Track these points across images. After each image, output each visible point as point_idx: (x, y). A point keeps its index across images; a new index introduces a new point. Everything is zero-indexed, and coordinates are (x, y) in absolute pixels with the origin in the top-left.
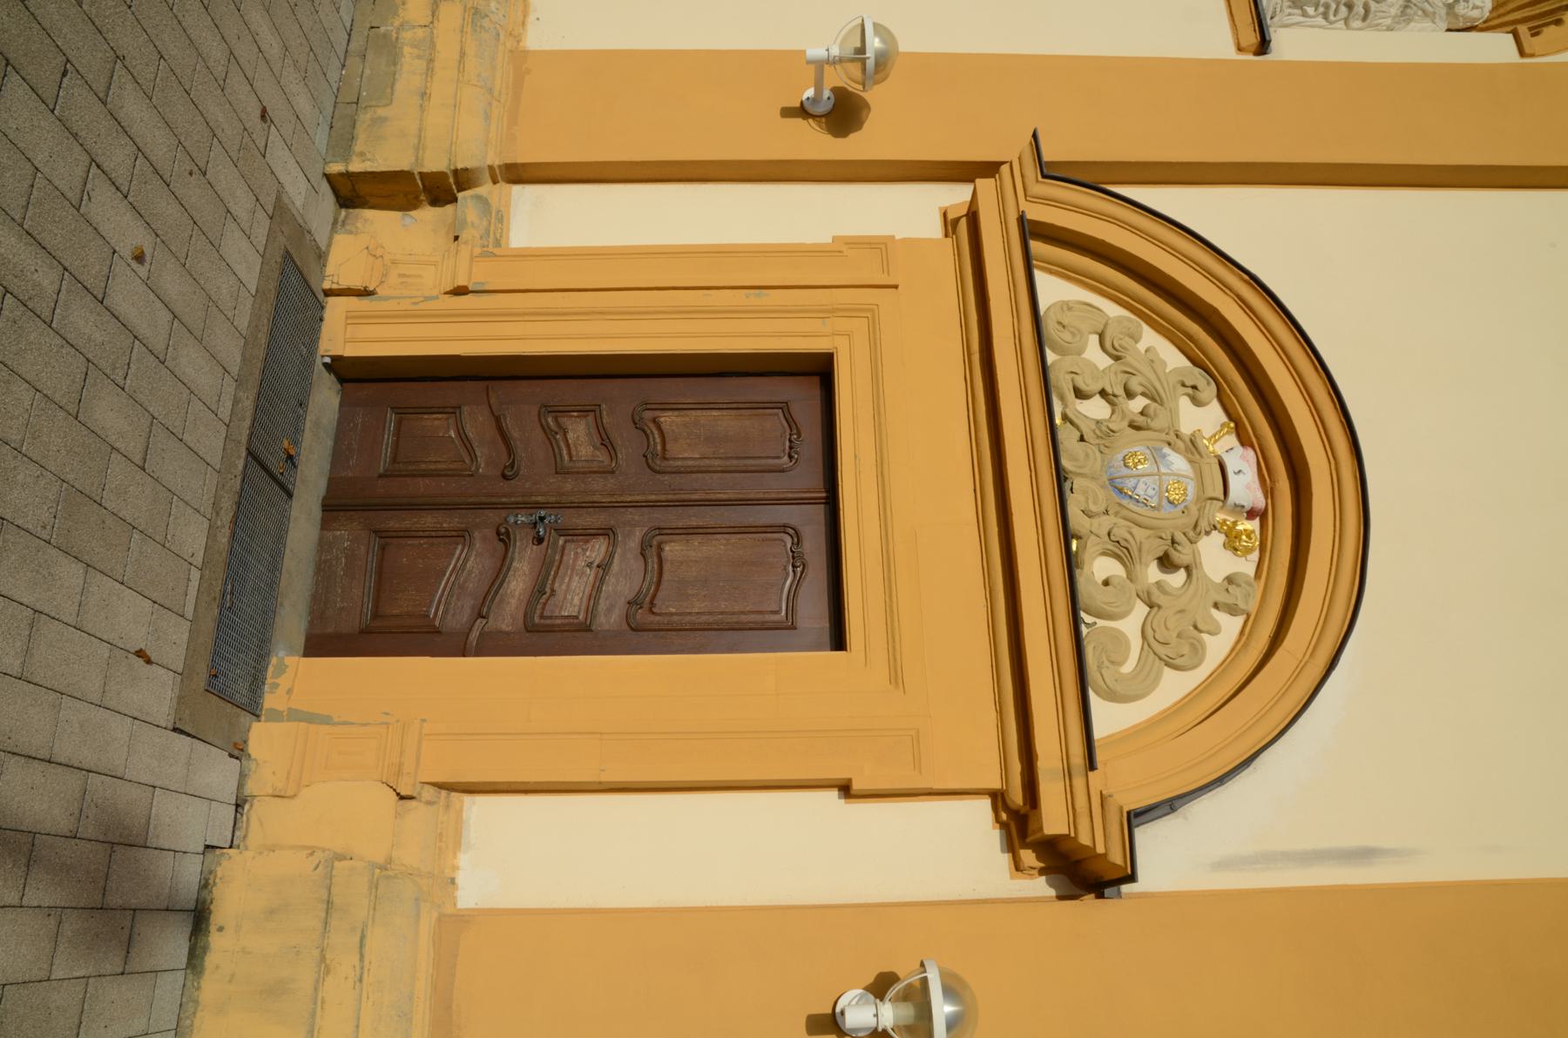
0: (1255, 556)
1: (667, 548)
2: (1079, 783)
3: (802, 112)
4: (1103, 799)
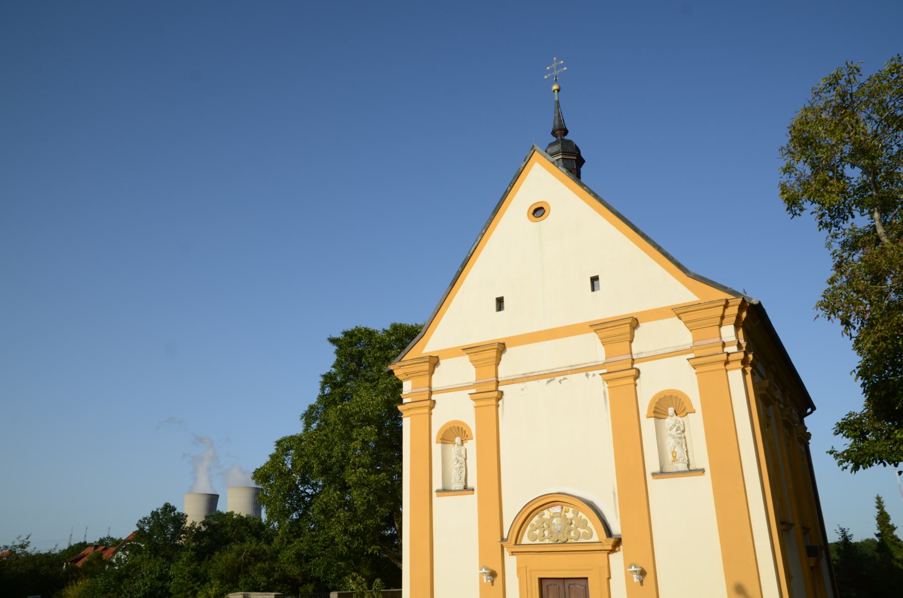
3: (492, 582)
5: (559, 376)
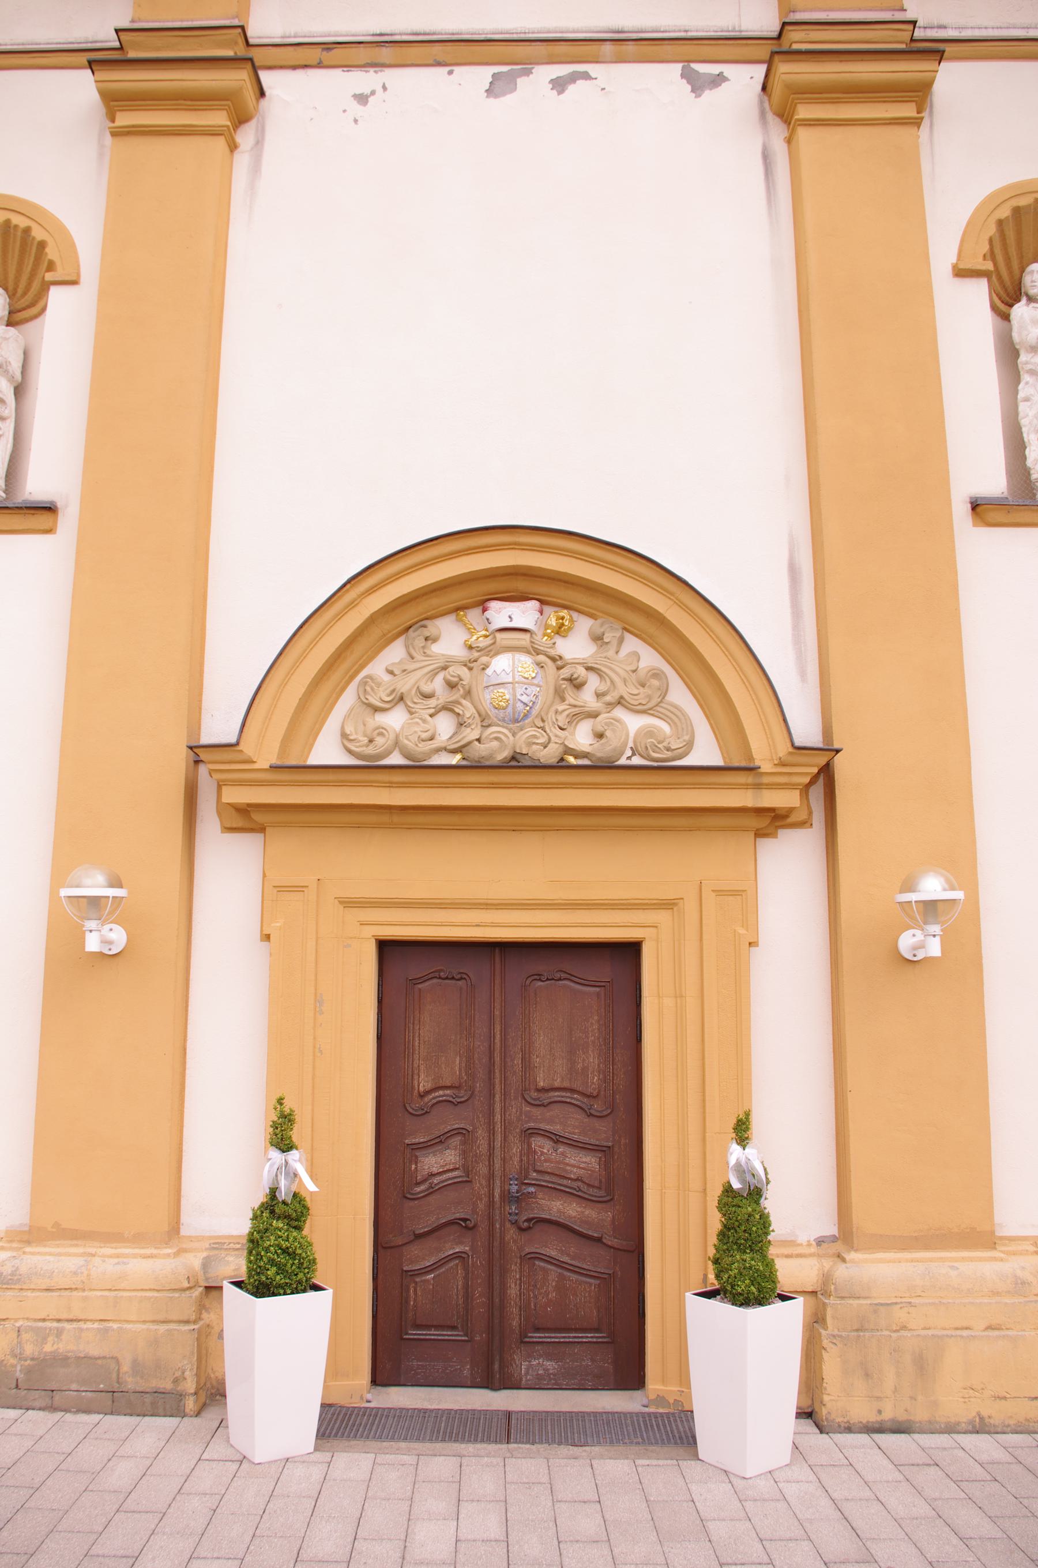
0: (575, 615)
1: (542, 1084)
2: (766, 780)
4: (782, 764)
5: (551, 61)
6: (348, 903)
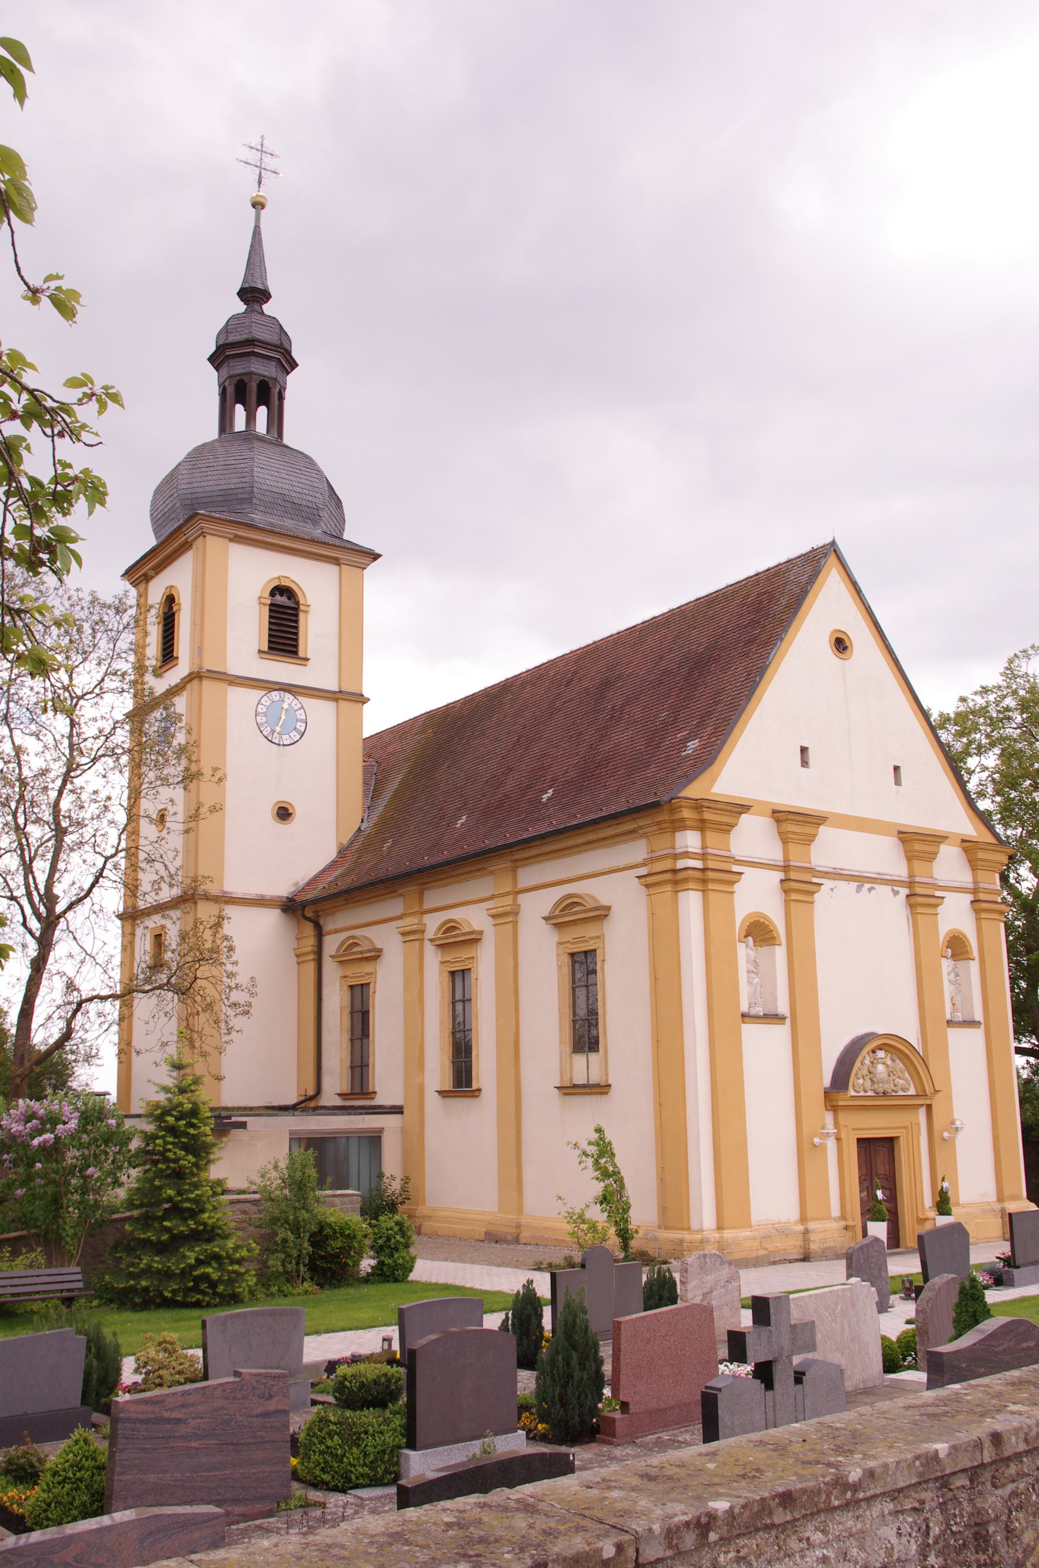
6: (854, 1129)
